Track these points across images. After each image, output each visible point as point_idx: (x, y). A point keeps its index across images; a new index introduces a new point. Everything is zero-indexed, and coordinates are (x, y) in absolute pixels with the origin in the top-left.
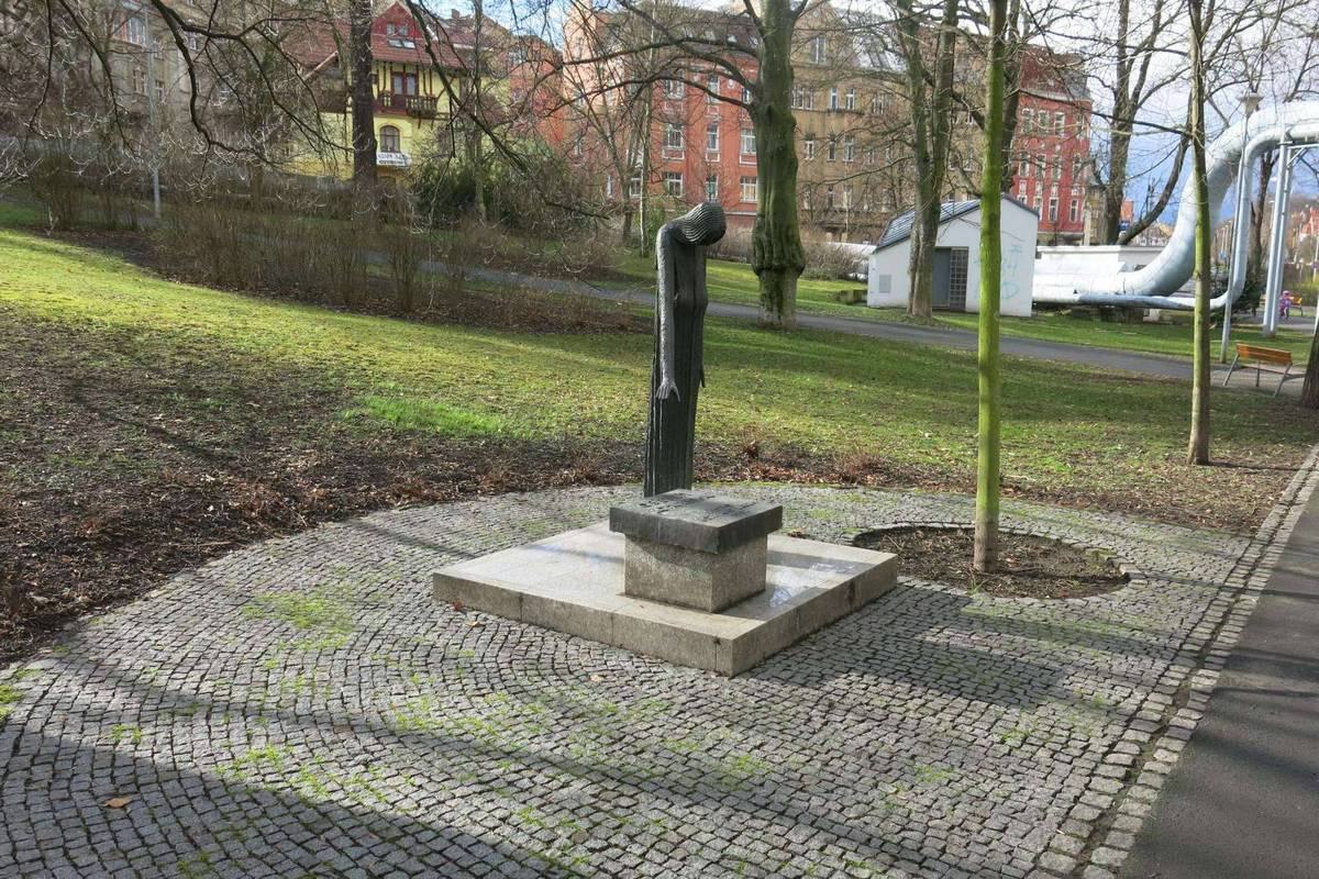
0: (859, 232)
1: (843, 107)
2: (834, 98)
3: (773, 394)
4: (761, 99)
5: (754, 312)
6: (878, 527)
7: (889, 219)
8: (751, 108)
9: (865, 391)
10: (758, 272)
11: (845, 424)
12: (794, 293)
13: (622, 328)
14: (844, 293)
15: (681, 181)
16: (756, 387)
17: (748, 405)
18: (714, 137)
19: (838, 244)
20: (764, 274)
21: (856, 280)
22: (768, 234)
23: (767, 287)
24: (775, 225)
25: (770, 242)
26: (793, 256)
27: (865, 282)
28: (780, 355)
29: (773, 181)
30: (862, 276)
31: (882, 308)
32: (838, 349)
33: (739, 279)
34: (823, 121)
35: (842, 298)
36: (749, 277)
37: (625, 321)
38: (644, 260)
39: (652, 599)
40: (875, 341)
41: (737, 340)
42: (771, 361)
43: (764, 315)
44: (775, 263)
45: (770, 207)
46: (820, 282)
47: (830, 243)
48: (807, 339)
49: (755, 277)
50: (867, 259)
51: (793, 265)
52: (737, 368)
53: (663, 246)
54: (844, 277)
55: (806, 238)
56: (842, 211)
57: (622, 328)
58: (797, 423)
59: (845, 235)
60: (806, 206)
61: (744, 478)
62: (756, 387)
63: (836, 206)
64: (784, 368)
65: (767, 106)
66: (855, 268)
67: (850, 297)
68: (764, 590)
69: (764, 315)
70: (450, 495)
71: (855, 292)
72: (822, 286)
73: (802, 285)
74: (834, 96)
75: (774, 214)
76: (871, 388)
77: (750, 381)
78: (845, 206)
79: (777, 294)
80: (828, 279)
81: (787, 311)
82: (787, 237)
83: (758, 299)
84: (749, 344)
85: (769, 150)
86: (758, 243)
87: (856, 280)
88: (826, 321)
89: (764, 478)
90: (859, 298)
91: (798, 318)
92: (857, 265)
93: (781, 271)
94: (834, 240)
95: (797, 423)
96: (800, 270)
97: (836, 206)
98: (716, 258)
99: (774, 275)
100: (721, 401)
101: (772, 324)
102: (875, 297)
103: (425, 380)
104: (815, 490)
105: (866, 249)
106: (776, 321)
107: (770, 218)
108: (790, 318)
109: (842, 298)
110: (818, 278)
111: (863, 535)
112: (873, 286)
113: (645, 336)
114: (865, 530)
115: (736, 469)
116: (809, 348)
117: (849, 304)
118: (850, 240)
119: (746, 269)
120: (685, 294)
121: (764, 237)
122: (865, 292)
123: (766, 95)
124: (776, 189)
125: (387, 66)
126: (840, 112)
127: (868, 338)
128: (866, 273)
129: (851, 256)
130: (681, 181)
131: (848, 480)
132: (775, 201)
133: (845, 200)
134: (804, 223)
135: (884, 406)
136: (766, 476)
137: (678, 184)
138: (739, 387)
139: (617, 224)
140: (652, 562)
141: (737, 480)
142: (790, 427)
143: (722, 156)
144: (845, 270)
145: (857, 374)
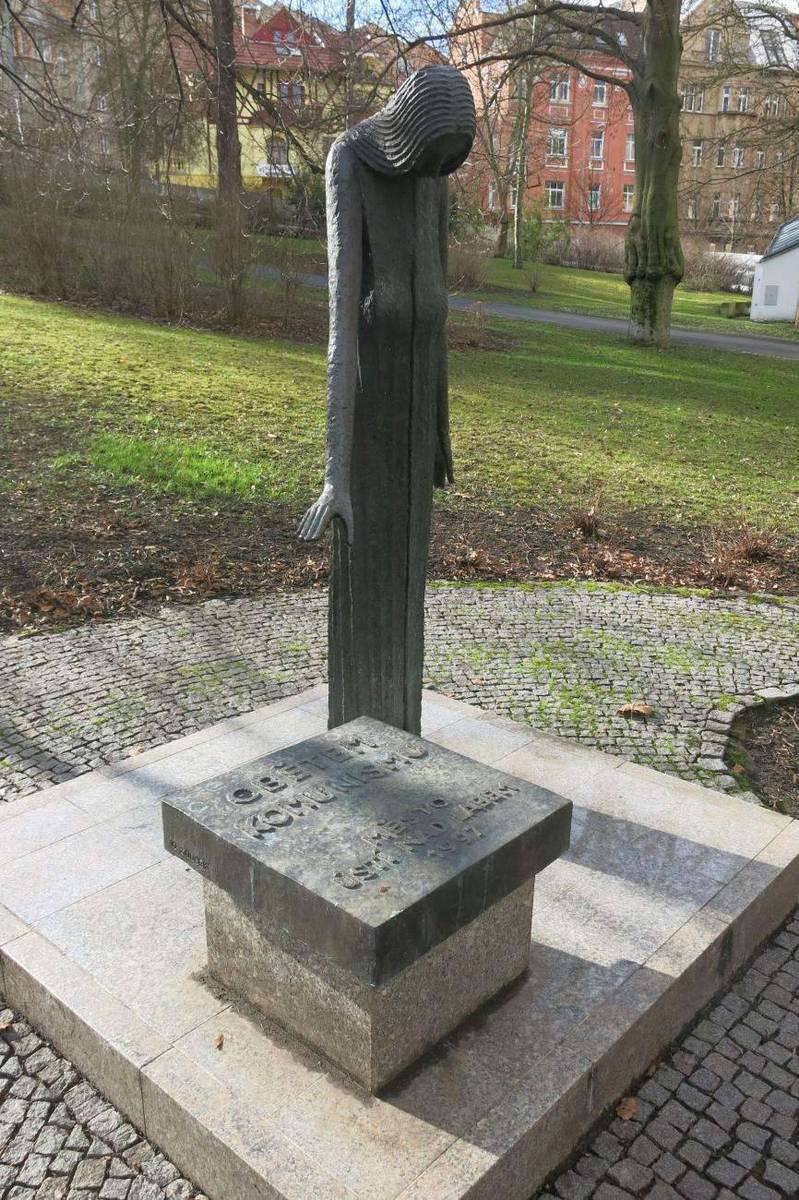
0: (741, 243)
1: (735, 109)
2: (726, 99)
3: (633, 428)
4: (642, 75)
5: (625, 326)
6: (771, 693)
7: (777, 227)
8: (630, 88)
9: (745, 425)
10: (630, 281)
11: (720, 473)
12: (669, 305)
13: (473, 344)
14: (725, 305)
15: (563, 191)
16: (613, 419)
17: (598, 446)
18: (599, 143)
19: (721, 255)
20: (636, 283)
21: (738, 292)
22: (643, 237)
23: (639, 298)
24: (652, 226)
25: (645, 246)
26: (671, 262)
27: (749, 294)
28: (646, 376)
29: (652, 174)
30: (745, 288)
31: (766, 322)
32: (714, 370)
33: (615, 290)
34: (714, 125)
35: (723, 311)
36: (623, 287)
37: (475, 337)
38: (515, 271)
39: (254, 1012)
40: (758, 360)
41: (601, 359)
42: (636, 387)
43: (636, 330)
44: (649, 270)
45: (647, 205)
46: (701, 294)
47: (715, 254)
48: (682, 358)
49: (628, 287)
50: (751, 269)
51: (671, 273)
52: (593, 394)
53: (336, 182)
54: (726, 289)
55: (688, 248)
56: (728, 220)
57: (473, 344)
58: (658, 474)
59: (729, 246)
60: (691, 216)
61: (569, 574)
62: (613, 419)
63: (721, 215)
64: (651, 393)
65: (649, 84)
66: (738, 279)
67: (732, 311)
68: (523, 977)
69: (636, 330)
70: (118, 604)
71: (738, 304)
72: (701, 299)
73: (680, 296)
74: (729, 95)
75: (652, 213)
76: (754, 421)
77: (607, 412)
78: (731, 215)
79: (649, 307)
80: (709, 291)
81: (660, 325)
82: (665, 240)
83: (629, 311)
84: (613, 362)
85: (650, 134)
86: (632, 247)
87: (738, 292)
88: (706, 336)
89: (598, 576)
90: (742, 312)
91: (673, 333)
92: (741, 276)
93: (655, 279)
94: (718, 249)
95: (658, 474)
96: (678, 279)
97: (721, 215)
98: (593, 269)
99: (647, 284)
100: (565, 440)
101: (642, 340)
102: (759, 310)
103: (205, 417)
104: (673, 602)
105: (751, 258)
106: (647, 336)
107: (646, 218)
108: (664, 333)
109: (723, 311)
110: (698, 290)
111: (748, 710)
112: (757, 298)
113: (497, 354)
114: (749, 700)
115: (561, 557)
116: (676, 372)
117: (730, 317)
118: (734, 250)
119: (619, 279)
120: (388, 292)
121: (638, 240)
122: (749, 305)
123: (649, 71)
124: (656, 183)
125: (274, 73)
126: (732, 115)
127: (750, 357)
128: (751, 285)
129: (736, 267)
130: (563, 191)
131: (723, 583)
132: (653, 198)
133: (732, 209)
134: (687, 234)
135: (771, 446)
136: (605, 572)
137: (560, 194)
138: (593, 420)
139: (493, 234)
140: (253, 935)
141: (558, 578)
142: (648, 478)
143: (607, 164)
144: (727, 280)
145: (737, 403)
